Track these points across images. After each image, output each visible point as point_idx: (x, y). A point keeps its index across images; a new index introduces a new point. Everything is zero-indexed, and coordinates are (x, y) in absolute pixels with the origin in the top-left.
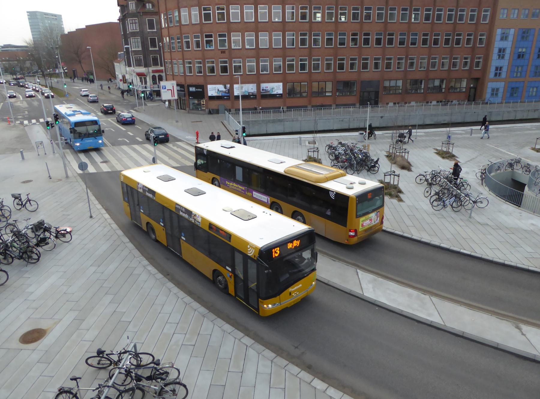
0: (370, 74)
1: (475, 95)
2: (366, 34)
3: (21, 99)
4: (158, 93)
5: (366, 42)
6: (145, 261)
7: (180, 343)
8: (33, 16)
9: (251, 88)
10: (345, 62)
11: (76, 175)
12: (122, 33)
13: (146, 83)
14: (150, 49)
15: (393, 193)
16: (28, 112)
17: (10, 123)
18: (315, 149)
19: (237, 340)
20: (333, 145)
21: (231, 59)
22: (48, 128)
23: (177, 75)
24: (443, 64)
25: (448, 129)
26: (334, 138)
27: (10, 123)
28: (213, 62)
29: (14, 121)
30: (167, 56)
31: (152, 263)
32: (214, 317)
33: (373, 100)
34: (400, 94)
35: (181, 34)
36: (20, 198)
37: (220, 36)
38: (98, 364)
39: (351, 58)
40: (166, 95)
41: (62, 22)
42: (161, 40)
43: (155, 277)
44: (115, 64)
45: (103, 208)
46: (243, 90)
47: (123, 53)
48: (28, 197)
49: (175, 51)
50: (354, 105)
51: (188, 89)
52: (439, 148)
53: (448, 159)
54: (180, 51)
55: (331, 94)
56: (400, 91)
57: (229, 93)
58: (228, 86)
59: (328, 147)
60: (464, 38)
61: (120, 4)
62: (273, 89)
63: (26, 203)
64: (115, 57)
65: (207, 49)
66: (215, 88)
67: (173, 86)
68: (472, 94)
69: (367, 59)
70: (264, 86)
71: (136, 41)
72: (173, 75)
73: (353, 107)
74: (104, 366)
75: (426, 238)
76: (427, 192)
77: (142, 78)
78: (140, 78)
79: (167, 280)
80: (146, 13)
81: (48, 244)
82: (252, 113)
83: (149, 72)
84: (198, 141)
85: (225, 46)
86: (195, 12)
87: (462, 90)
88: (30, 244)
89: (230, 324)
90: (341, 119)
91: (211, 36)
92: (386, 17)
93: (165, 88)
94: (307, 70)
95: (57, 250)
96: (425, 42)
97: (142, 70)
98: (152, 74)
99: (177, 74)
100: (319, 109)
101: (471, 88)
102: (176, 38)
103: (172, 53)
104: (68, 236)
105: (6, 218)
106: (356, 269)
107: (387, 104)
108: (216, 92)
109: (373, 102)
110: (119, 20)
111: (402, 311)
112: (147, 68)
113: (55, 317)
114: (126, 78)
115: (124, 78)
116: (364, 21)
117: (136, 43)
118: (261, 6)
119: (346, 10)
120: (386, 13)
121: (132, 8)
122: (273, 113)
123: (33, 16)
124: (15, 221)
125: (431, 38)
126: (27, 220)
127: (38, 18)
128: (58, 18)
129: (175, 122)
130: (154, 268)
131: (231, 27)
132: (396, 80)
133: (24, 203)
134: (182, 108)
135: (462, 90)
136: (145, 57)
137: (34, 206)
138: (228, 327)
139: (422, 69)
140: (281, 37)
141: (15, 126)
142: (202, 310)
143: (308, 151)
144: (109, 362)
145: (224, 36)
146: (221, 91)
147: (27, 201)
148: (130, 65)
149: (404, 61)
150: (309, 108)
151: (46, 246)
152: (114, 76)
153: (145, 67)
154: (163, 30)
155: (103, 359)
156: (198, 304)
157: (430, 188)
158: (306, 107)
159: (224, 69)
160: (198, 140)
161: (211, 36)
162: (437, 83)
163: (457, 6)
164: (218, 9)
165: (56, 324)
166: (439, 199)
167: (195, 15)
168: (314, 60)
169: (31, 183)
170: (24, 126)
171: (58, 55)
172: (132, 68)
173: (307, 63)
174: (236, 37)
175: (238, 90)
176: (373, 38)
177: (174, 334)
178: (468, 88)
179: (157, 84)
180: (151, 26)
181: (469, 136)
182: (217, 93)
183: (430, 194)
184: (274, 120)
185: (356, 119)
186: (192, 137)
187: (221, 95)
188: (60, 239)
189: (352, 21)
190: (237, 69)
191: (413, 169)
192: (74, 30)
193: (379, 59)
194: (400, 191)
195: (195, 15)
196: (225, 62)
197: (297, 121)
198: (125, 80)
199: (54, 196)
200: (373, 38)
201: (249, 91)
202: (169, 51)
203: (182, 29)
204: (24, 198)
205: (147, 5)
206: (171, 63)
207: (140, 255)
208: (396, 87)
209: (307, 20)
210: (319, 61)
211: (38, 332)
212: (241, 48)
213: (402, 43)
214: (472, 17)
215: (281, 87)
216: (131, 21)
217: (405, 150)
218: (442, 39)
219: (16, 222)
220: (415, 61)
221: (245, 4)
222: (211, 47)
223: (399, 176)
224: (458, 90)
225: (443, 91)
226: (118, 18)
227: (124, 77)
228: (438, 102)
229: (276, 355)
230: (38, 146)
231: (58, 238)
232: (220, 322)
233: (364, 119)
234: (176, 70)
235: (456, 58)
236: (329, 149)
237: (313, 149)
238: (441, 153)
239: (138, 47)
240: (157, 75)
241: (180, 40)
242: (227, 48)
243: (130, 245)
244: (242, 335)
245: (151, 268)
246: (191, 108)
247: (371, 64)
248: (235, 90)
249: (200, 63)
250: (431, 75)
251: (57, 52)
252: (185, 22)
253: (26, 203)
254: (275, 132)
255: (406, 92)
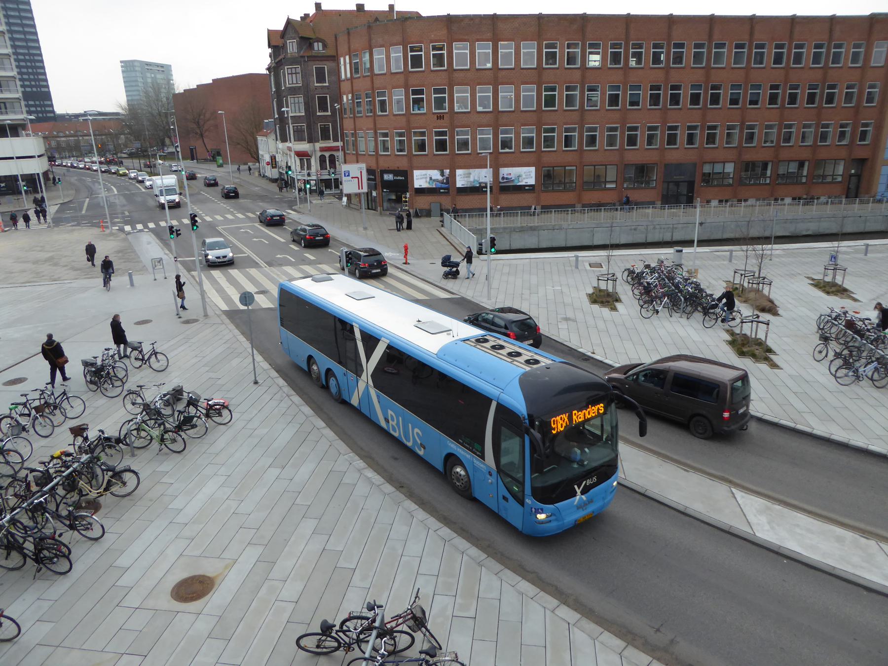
0: (679, 153)
1: (858, 187)
2: (673, 88)
3: (116, 193)
4: (337, 183)
5: (675, 99)
6: (358, 462)
7: (449, 613)
8: (129, 67)
9: (483, 176)
10: (597, 133)
11: (219, 312)
12: (274, 90)
13: (309, 167)
14: (318, 114)
15: (757, 352)
16: (129, 212)
17: (104, 230)
18: (610, 276)
19: (548, 612)
20: (635, 269)
21: (452, 127)
22: (172, 236)
23: (365, 155)
24: (803, 137)
25: (836, 244)
26: (636, 258)
27: (104, 230)
28: (423, 134)
29: (110, 226)
30: (348, 124)
31: (370, 466)
32: (498, 567)
33: (684, 195)
34: (730, 185)
35: (373, 89)
36: (140, 349)
37: (437, 91)
38: (318, 647)
39: (668, 127)
40: (349, 187)
41: (172, 75)
42: (339, 100)
43: (381, 489)
44: (259, 138)
45: (273, 368)
46: (472, 179)
47: (273, 120)
48: (153, 348)
49: (362, 117)
50: (651, 203)
51: (382, 177)
52: (819, 277)
53: (836, 295)
54: (371, 116)
55: (613, 186)
56: (731, 181)
57: (447, 183)
58: (447, 172)
59: (626, 273)
60: (840, 92)
61: (273, 44)
62: (519, 176)
63: (149, 358)
64: (258, 127)
65: (414, 112)
66: (426, 175)
67: (361, 172)
68: (853, 186)
69: (714, 128)
70: (504, 171)
71: (296, 101)
72: (357, 155)
73: (653, 207)
74: (325, 650)
75: (839, 434)
76: (820, 352)
77: (303, 159)
78: (300, 159)
79: (403, 496)
80: (315, 57)
81: (196, 426)
82: (523, 214)
83: (315, 151)
84: (406, 261)
85: (442, 108)
86: (397, 53)
87: (836, 179)
88: (167, 425)
89: (528, 581)
90: (633, 227)
91: (421, 92)
92: (709, 60)
93: (348, 176)
94: (575, 147)
95: (210, 437)
96: (773, 99)
97: (304, 146)
98: (319, 154)
99: (363, 153)
100: (594, 210)
101: (851, 175)
102: (363, 96)
103: (356, 119)
104: (225, 412)
105: (121, 380)
106: (730, 487)
107: (708, 202)
108: (426, 182)
109: (684, 199)
110: (268, 69)
111: (834, 568)
112: (311, 144)
113: (226, 555)
114: (277, 160)
115: (274, 161)
116: (671, 65)
117: (297, 105)
118: (502, 43)
119: (621, 48)
120: (709, 52)
121: (291, 50)
122: (521, 216)
123: (129, 67)
124: (141, 387)
125: (783, 93)
126: (158, 386)
127: (136, 71)
128: (165, 69)
129: (362, 229)
130: (376, 474)
131: (453, 78)
132: (724, 163)
133: (146, 357)
134: (370, 207)
135: (836, 179)
136: (309, 127)
137: (163, 362)
138: (525, 586)
139: (768, 144)
140: (535, 94)
141: (111, 234)
142: (474, 551)
143: (598, 280)
144: (336, 644)
145: (443, 91)
146: (434, 180)
147: (151, 355)
148: (284, 139)
149: (737, 131)
150: (578, 208)
151: (192, 430)
152: (255, 156)
153: (309, 142)
154: (342, 84)
155: (329, 639)
156: (464, 541)
157: (826, 345)
158: (573, 206)
159: (441, 145)
160: (407, 259)
161: (421, 92)
162: (793, 168)
163: (830, 39)
164: (434, 48)
165: (229, 567)
166: (847, 365)
167: (397, 59)
168: (546, 131)
169: (136, 321)
170: (126, 235)
171: (173, 124)
172: (288, 144)
173: (575, 135)
174: (461, 94)
175: (462, 179)
176: (685, 94)
177: (435, 596)
178: (848, 177)
179: (326, 169)
180: (321, 78)
181: (862, 256)
182: (429, 183)
183: (826, 356)
184: (522, 227)
185: (658, 227)
186: (395, 254)
187: (434, 187)
188: (213, 418)
189: (651, 66)
190: (464, 144)
191: (780, 312)
192: (193, 86)
193: (695, 128)
194: (770, 350)
195: (397, 59)
196: (443, 133)
197: (560, 229)
198: (274, 163)
199: (190, 346)
200: (685, 94)
201: (481, 181)
202: (352, 116)
203: (375, 81)
204: (147, 349)
205: (316, 44)
206: (354, 135)
207: (349, 450)
208: (723, 175)
209: (578, 66)
210: (554, 132)
211: (201, 582)
212: (469, 110)
213: (734, 101)
214: (856, 56)
215: (533, 174)
216: (289, 70)
217: (764, 279)
218: (802, 94)
219: (141, 389)
220: (756, 131)
221: (478, 40)
222: (422, 109)
223: (768, 324)
224: (829, 179)
225: (804, 180)
226: (267, 67)
227: (273, 158)
228: (794, 199)
229: (626, 644)
230: (155, 266)
231: (211, 417)
232: (508, 575)
233: (671, 226)
234: (362, 147)
235: (827, 126)
236: (628, 276)
237: (606, 276)
238: (822, 285)
239: (300, 112)
240: (327, 154)
241: (371, 99)
242: (447, 111)
243: (329, 433)
244: (555, 602)
245: (370, 474)
246: (385, 208)
247: (681, 136)
248: (458, 179)
249: (401, 135)
250: (784, 155)
251: (173, 119)
252: (396, 69)
253: (149, 358)
254: (523, 248)
255: (740, 182)
